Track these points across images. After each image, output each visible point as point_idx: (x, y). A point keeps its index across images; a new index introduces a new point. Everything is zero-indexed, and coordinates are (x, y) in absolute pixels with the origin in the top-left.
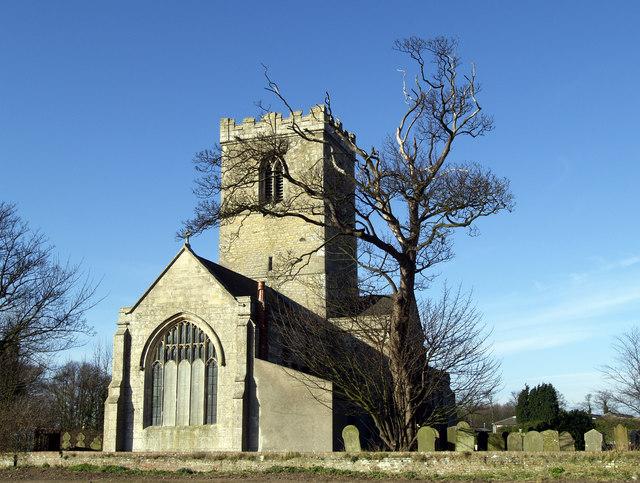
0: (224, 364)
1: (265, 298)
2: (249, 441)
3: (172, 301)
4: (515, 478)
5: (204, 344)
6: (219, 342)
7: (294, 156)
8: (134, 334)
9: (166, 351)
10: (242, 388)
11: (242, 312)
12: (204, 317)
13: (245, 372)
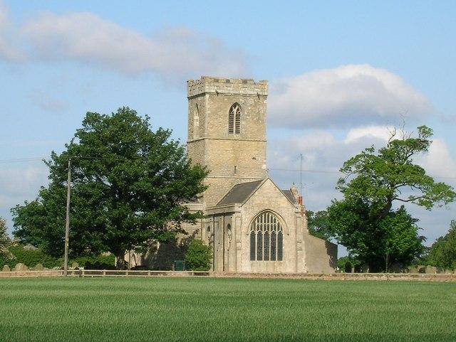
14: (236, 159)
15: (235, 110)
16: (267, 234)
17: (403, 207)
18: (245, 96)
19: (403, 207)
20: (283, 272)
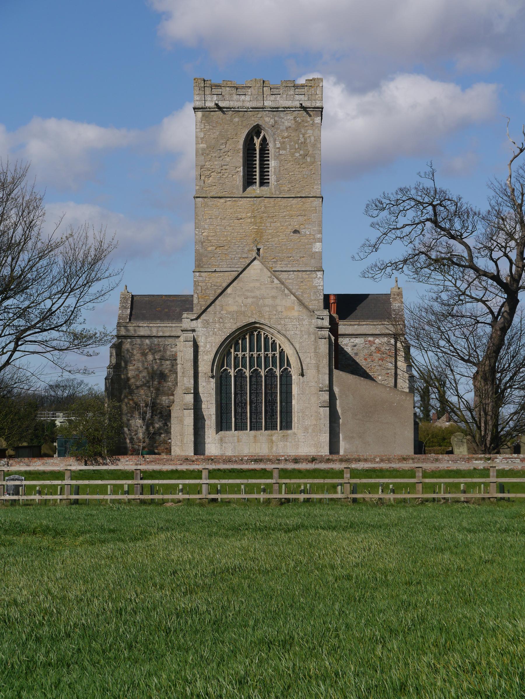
3: (243, 309)
4: (111, 414)
7: (286, 134)
8: (201, 343)
10: (326, 397)
12: (279, 327)
14: (260, 233)
15: (257, 142)
16: (255, 374)
17: (244, 190)
18: (275, 110)
19: (244, 190)
20: (292, 452)
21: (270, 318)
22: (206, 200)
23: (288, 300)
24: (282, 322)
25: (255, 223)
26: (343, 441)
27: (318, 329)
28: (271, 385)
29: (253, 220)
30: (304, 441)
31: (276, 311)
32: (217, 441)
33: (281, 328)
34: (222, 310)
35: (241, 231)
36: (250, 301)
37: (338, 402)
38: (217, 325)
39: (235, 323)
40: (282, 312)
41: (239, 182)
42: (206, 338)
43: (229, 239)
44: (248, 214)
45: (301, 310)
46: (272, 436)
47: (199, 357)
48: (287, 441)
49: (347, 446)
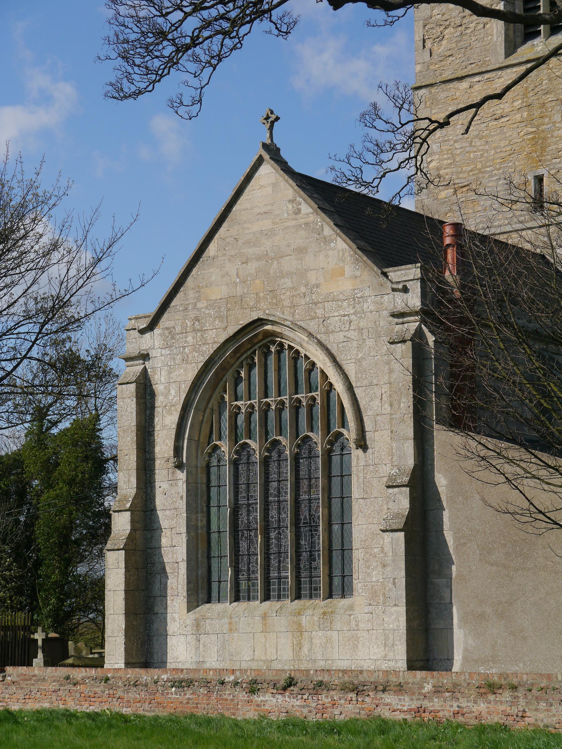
0: (362, 445)
1: (463, 267)
2: (426, 646)
3: (239, 291)
5: (317, 394)
6: (350, 388)
9: (234, 416)
10: (402, 502)
11: (400, 307)
12: (312, 326)
13: (410, 462)
21: (293, 306)
22: (433, 90)
23: (330, 253)
24: (320, 312)
25: (529, 121)
26: (460, 627)
27: (396, 320)
28: (310, 479)
29: (525, 115)
30: (370, 626)
31: (306, 285)
32: (189, 628)
33: (316, 327)
34: (198, 299)
35: (502, 144)
36: (252, 267)
37: (446, 515)
38: (190, 339)
39: (225, 329)
40: (318, 286)
41: (498, 37)
42: (170, 373)
43: (479, 166)
44: (516, 104)
45: (358, 273)
46: (299, 614)
47: (156, 419)
48: (331, 629)
49: (471, 642)
